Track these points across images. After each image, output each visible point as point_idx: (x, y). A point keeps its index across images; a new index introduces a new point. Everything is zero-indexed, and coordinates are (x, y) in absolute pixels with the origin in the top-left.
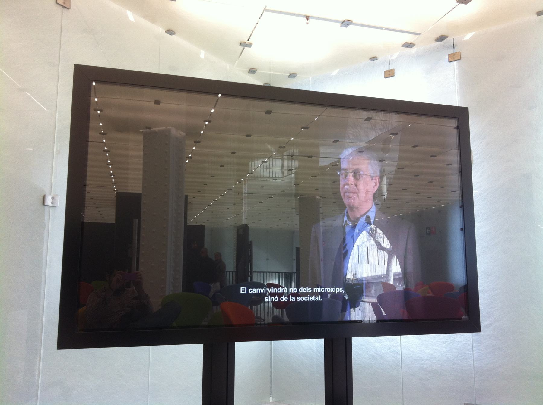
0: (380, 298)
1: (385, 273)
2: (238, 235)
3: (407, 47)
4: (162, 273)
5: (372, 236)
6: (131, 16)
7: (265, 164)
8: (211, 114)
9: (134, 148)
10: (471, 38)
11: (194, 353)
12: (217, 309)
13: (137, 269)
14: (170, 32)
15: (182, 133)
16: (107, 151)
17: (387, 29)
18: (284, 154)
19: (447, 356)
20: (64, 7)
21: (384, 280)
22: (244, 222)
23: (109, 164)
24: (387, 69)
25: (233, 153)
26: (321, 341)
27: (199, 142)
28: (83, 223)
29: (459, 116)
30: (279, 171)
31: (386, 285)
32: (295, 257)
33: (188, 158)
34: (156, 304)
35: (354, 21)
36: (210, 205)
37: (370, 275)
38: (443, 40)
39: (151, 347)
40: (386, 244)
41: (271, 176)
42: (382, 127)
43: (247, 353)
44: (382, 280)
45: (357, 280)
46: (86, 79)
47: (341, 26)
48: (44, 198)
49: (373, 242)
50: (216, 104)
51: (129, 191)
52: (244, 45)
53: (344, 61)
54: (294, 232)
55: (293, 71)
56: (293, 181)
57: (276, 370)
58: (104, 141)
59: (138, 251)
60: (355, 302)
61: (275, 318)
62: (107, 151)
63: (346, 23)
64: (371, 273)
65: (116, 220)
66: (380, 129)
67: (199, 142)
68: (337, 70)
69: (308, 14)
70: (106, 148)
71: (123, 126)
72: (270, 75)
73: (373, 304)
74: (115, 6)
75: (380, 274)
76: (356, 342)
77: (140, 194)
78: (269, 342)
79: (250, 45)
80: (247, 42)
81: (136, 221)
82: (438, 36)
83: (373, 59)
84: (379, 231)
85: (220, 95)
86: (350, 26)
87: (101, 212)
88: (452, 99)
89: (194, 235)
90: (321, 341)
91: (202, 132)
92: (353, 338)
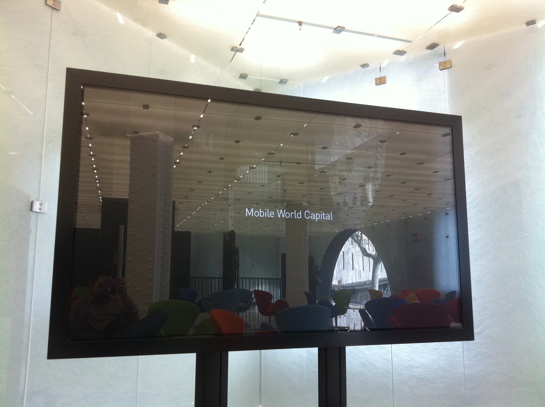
0: (367, 305)
1: (371, 279)
2: (225, 242)
3: (399, 54)
4: (147, 282)
5: (357, 242)
6: (121, 18)
7: (255, 170)
8: (200, 119)
9: (120, 155)
10: (462, 46)
11: (185, 364)
12: (204, 316)
13: (123, 275)
14: (161, 36)
15: (169, 138)
16: (93, 156)
17: (379, 36)
18: (271, 160)
19: (438, 363)
20: (53, 8)
21: (369, 287)
22: (231, 228)
23: (94, 169)
24: (378, 76)
25: (223, 159)
26: (315, 351)
27: (187, 147)
28: (75, 229)
29: (452, 124)
30: (266, 177)
31: (372, 292)
32: (280, 264)
33: (176, 163)
34: (143, 312)
35: (346, 28)
36: (197, 211)
37: (355, 281)
38: (434, 48)
39: (140, 356)
40: (371, 249)
41: (258, 182)
42: (367, 134)
43: (238, 361)
44: (367, 287)
45: (343, 286)
46: (79, 83)
47: (334, 32)
48: (32, 203)
49: (358, 249)
50: (205, 110)
51: (114, 197)
52: (236, 50)
53: (337, 68)
54: (279, 238)
55: (284, 77)
56: (280, 187)
57: (272, 380)
58: (90, 145)
59: (124, 258)
60: (342, 310)
61: (264, 325)
62: (93, 156)
63: (339, 30)
64: (356, 279)
65: (102, 227)
66: (366, 136)
67: (187, 147)
68: (328, 77)
69: (300, 20)
70: (92, 153)
71: (108, 131)
72: (261, 81)
73: (361, 311)
74: (104, 8)
75: (365, 280)
76: (349, 349)
77: (126, 200)
78: (258, 351)
79: (241, 50)
80: (239, 47)
81: (122, 227)
82: (428, 44)
83: (364, 66)
84: (365, 237)
85: (209, 101)
86: (343, 33)
87: (89, 219)
88: (443, 107)
89: (182, 243)
90: (315, 351)
91: (191, 137)
92: (347, 347)
